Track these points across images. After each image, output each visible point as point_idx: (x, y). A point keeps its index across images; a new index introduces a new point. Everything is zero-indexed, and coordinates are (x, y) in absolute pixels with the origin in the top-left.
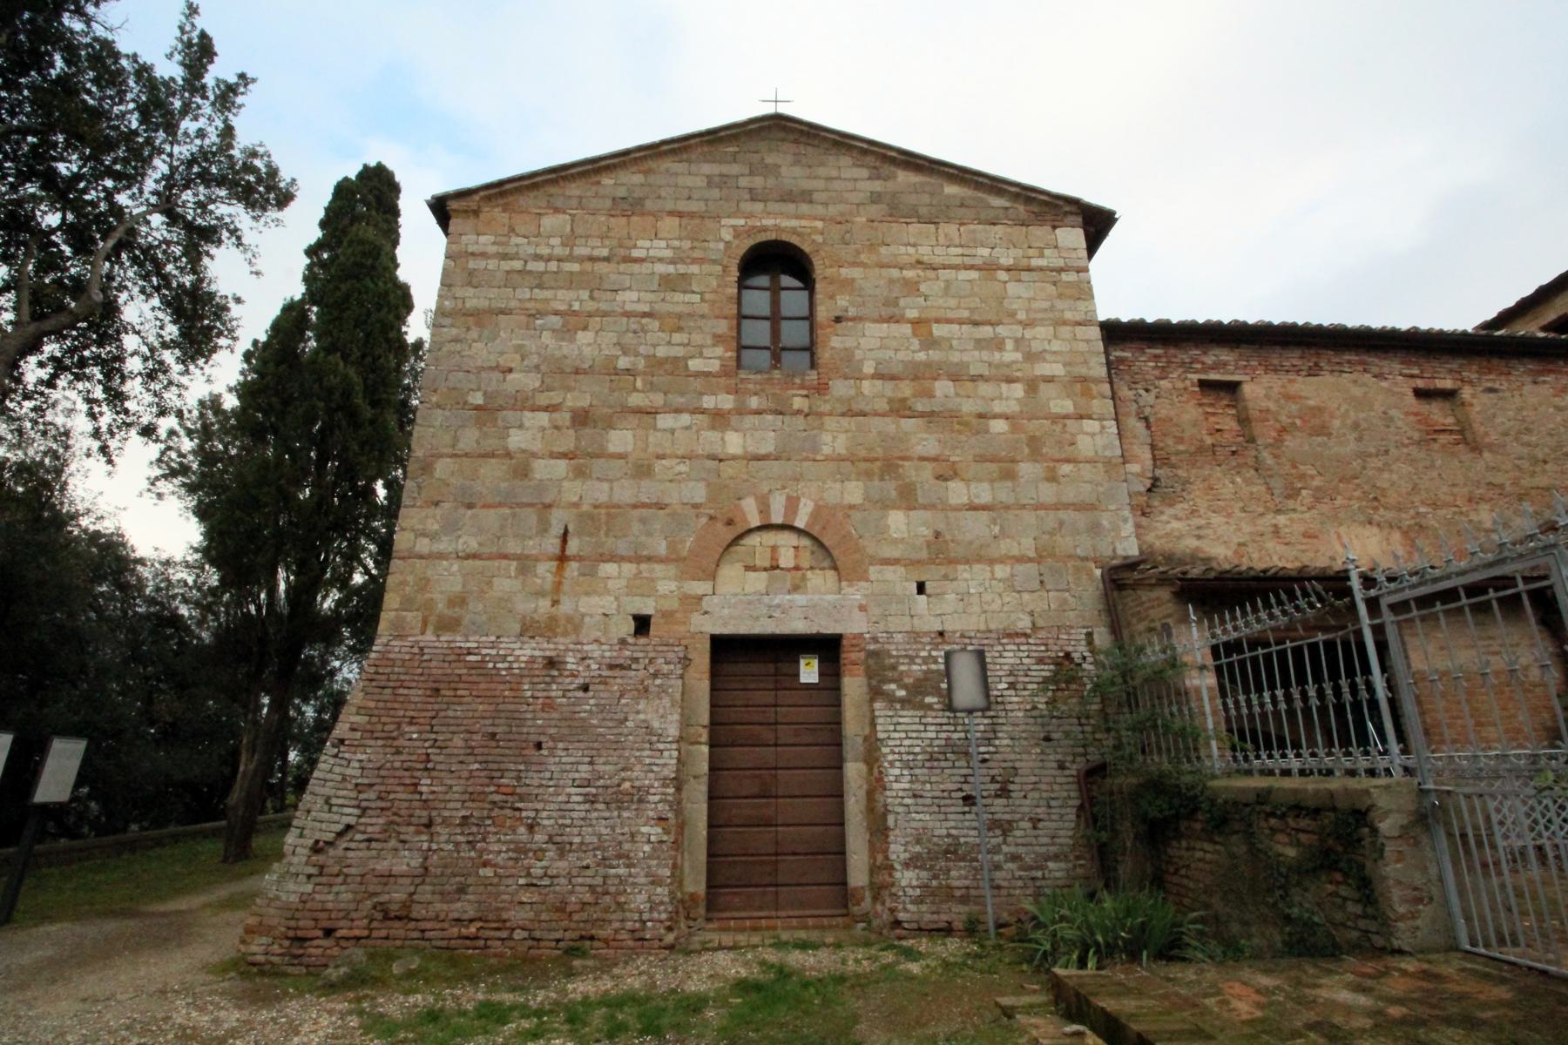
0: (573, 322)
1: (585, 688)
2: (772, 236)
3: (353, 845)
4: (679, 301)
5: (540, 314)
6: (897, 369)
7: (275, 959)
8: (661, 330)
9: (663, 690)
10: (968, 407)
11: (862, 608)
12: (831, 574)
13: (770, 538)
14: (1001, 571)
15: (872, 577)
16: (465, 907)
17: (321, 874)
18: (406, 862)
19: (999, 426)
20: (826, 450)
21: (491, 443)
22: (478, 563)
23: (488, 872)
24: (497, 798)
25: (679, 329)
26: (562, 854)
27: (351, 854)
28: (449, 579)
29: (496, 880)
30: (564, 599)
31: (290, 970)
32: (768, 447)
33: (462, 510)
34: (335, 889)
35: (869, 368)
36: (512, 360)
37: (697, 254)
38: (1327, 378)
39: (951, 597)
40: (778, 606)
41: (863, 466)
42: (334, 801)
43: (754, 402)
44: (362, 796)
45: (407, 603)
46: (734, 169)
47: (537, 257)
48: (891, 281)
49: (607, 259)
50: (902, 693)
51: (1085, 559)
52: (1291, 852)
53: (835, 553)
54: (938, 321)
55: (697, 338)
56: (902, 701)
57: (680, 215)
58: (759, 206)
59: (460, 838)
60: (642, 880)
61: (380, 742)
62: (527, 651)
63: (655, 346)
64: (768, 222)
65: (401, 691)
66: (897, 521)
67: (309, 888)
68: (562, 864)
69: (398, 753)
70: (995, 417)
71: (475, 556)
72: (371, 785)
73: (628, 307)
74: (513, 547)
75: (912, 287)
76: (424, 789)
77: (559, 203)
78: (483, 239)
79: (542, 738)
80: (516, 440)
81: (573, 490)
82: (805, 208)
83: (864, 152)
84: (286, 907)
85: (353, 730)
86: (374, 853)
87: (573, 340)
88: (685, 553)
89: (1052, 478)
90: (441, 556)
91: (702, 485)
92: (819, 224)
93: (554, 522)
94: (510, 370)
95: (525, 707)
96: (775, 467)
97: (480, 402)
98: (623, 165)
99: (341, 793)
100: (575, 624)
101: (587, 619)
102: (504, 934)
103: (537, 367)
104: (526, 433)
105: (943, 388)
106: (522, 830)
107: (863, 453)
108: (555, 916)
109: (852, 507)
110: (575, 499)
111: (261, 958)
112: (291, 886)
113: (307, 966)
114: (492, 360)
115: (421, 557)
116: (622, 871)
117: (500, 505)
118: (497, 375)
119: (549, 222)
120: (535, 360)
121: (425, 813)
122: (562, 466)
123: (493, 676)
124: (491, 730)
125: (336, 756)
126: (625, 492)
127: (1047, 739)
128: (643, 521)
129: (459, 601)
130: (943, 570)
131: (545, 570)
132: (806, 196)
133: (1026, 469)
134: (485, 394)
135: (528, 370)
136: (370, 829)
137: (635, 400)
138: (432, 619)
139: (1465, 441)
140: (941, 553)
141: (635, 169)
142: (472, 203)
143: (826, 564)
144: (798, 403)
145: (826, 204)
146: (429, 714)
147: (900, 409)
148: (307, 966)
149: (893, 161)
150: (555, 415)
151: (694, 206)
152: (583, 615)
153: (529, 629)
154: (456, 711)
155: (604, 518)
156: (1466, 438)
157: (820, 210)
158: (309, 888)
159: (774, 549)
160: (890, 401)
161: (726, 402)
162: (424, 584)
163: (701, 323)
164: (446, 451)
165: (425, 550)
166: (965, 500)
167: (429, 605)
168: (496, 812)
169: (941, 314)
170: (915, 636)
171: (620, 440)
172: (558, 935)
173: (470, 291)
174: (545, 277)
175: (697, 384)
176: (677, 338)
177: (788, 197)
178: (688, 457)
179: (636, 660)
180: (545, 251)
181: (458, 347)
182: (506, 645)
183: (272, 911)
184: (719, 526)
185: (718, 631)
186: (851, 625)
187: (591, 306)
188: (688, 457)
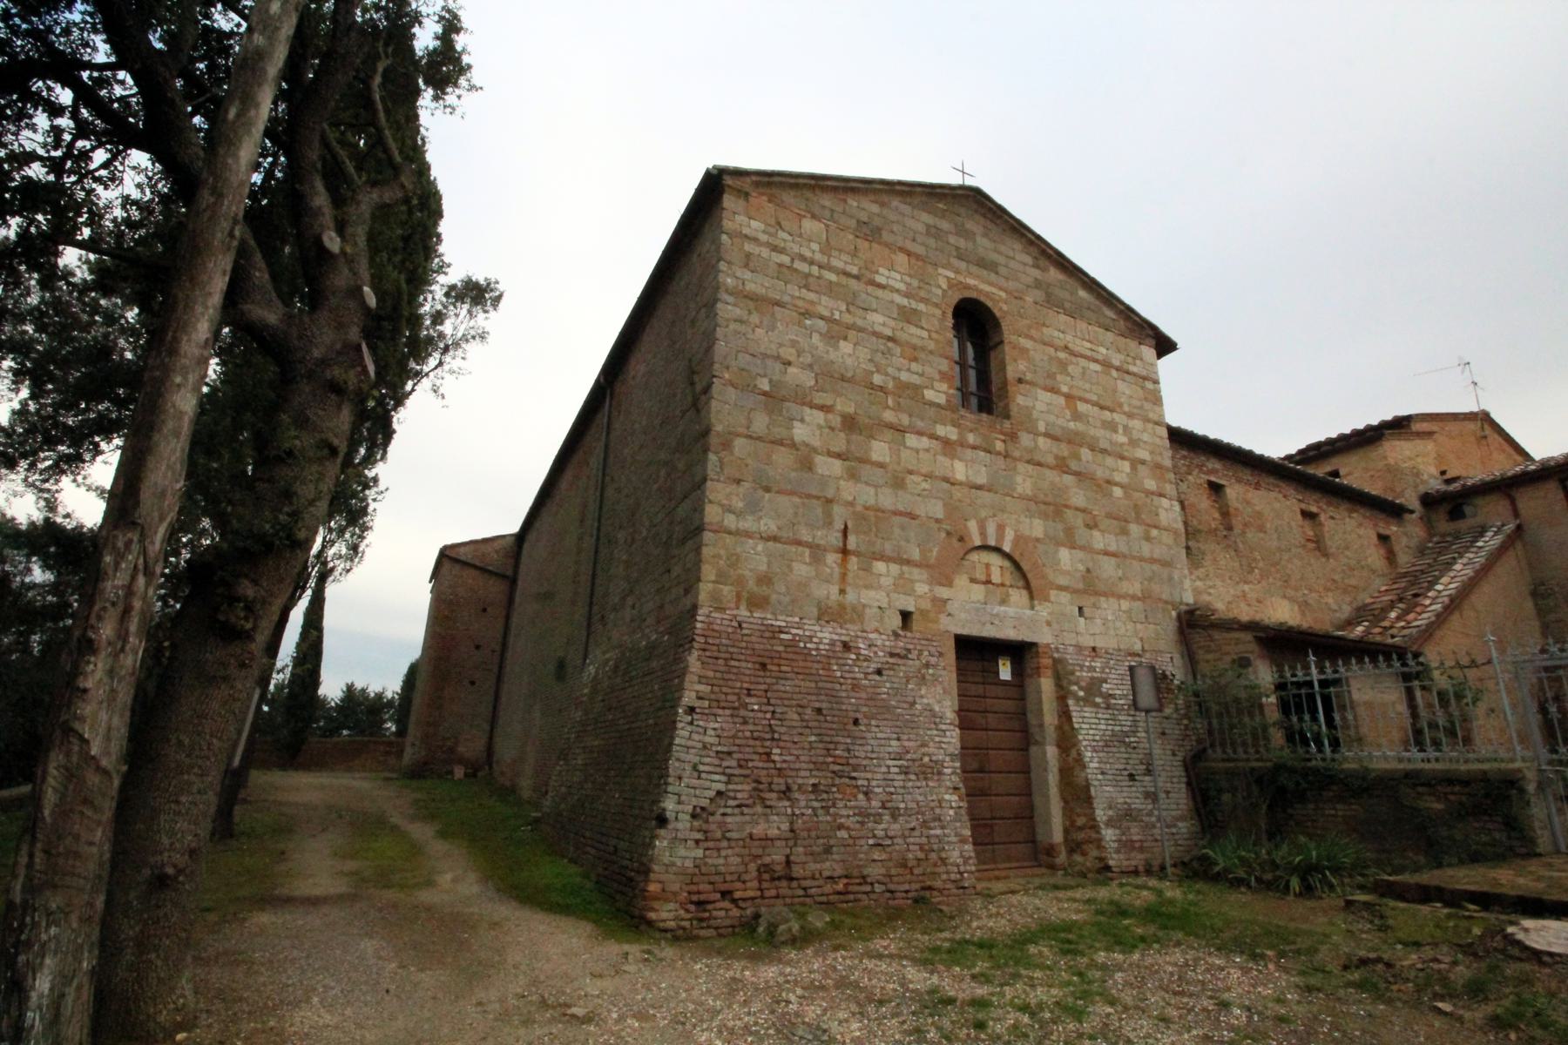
0: (836, 332)
1: (879, 672)
2: (974, 295)
3: (729, 811)
4: (914, 334)
5: (806, 314)
6: (1058, 432)
7: (686, 924)
8: (902, 356)
9: (935, 679)
10: (1100, 473)
11: (1049, 624)
12: (1024, 593)
13: (986, 557)
14: (1125, 605)
15: (1052, 599)
16: (830, 866)
17: (706, 840)
18: (776, 826)
19: (1118, 492)
20: (1020, 489)
21: (779, 432)
22: (779, 545)
23: (843, 834)
24: (837, 768)
25: (915, 359)
26: (894, 817)
27: (729, 819)
28: (757, 557)
29: (851, 842)
30: (848, 589)
31: (703, 933)
32: (982, 479)
33: (760, 492)
34: (723, 853)
35: (1042, 427)
36: (788, 353)
37: (922, 294)
38: (1262, 493)
39: (1098, 621)
40: (997, 615)
41: (1043, 507)
42: (701, 768)
43: (971, 438)
44: (725, 764)
45: (721, 578)
46: (945, 225)
47: (803, 258)
48: (1051, 358)
49: (857, 277)
50: (1081, 694)
51: (1166, 602)
52: (1439, 806)
53: (1029, 576)
54: (1081, 399)
55: (928, 370)
56: (1083, 699)
57: (909, 254)
58: (963, 265)
59: (816, 804)
60: (953, 839)
61: (728, 712)
62: (826, 635)
63: (899, 370)
64: (971, 282)
65: (733, 663)
66: (1064, 554)
67: (699, 853)
68: (896, 826)
69: (745, 723)
70: (1116, 484)
71: (775, 539)
72: (729, 753)
73: (878, 328)
74: (806, 536)
75: (1063, 365)
76: (776, 758)
77: (816, 210)
78: (754, 224)
79: (858, 715)
80: (800, 432)
81: (848, 490)
82: (993, 277)
83: (1031, 243)
84: (682, 872)
85: (700, 698)
86: (747, 818)
87: (836, 348)
88: (932, 561)
89: (1148, 538)
90: (748, 534)
91: (940, 504)
92: (1003, 294)
93: (837, 518)
94: (789, 363)
95: (838, 687)
96: (986, 497)
97: (767, 388)
98: (865, 192)
99: (707, 760)
100: (858, 613)
101: (867, 611)
102: (868, 888)
103: (811, 366)
104: (807, 428)
105: (1085, 453)
106: (861, 796)
107: (1042, 497)
108: (901, 871)
109: (1037, 540)
110: (850, 498)
111: (672, 924)
112: (682, 852)
113: (716, 928)
114: (773, 349)
115: (730, 533)
116: (938, 832)
117: (792, 493)
118: (778, 366)
119: (809, 225)
120: (809, 360)
121: (781, 781)
122: (837, 466)
123: (806, 654)
124: (817, 705)
125: (691, 723)
126: (887, 499)
127: (1163, 734)
128: (903, 528)
129: (765, 580)
130: (1093, 599)
131: (832, 558)
132: (992, 267)
133: (1135, 529)
134: (771, 381)
135: (803, 367)
136: (739, 795)
137: (888, 416)
138: (745, 594)
139: (1318, 549)
140: (1089, 589)
141: (872, 197)
142: (745, 184)
143: (1021, 583)
144: (999, 446)
145: (1007, 279)
146: (763, 687)
147: (1062, 466)
148: (716, 928)
149: (1049, 257)
150: (830, 416)
151: (920, 250)
152: (864, 606)
153: (827, 615)
154: (787, 686)
155: (872, 518)
156: (1318, 545)
157: (1002, 282)
158: (699, 853)
159: (988, 566)
160: (1056, 457)
161: (951, 433)
162: (735, 560)
163: (931, 358)
164: (740, 430)
165: (733, 527)
166: (1101, 546)
167: (740, 581)
168: (837, 781)
169: (1081, 394)
170: (1079, 648)
171: (879, 450)
172: (906, 887)
173: (748, 275)
174: (811, 280)
175: (932, 412)
176: (914, 366)
177: (983, 264)
178: (928, 476)
179: (909, 651)
180: (808, 254)
181: (742, 328)
182: (811, 627)
183: (673, 877)
184: (954, 541)
185: (960, 631)
186: (1044, 637)
187: (848, 319)
188: (928, 476)
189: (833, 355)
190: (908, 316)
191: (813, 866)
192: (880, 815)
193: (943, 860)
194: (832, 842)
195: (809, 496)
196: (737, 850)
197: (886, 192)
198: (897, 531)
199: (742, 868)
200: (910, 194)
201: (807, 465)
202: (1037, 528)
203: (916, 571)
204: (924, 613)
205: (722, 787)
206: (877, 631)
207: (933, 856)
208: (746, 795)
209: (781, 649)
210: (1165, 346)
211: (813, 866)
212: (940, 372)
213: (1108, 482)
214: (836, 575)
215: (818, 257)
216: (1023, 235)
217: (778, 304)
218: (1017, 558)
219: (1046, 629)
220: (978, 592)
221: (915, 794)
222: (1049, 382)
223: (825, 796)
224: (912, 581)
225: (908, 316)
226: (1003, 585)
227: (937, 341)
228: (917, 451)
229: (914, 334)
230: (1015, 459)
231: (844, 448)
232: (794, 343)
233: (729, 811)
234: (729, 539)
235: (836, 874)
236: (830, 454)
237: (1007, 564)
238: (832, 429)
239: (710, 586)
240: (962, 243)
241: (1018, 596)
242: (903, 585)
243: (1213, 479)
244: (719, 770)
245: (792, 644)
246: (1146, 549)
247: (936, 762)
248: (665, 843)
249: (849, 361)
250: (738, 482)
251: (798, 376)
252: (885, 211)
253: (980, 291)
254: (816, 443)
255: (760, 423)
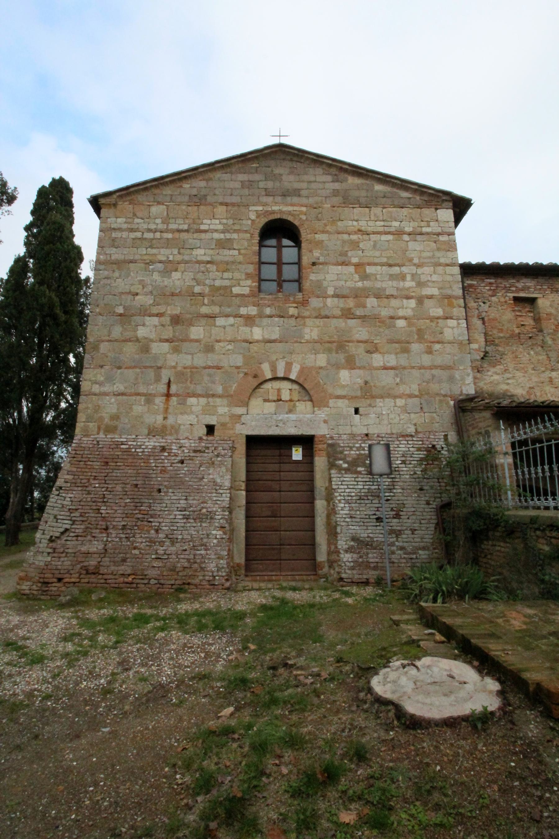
0: (170, 267)
1: (182, 462)
3: (69, 538)
4: (228, 254)
5: (152, 262)
6: (345, 292)
7: (35, 592)
9: (221, 463)
11: (325, 422)
14: (400, 402)
17: (54, 552)
18: (96, 546)
19: (401, 323)
20: (307, 337)
23: (136, 552)
25: (227, 270)
27: (68, 543)
28: (110, 406)
29: (141, 556)
32: (275, 336)
33: (115, 370)
34: (62, 559)
35: (330, 291)
36: (137, 288)
37: (237, 227)
41: (327, 345)
42: (59, 517)
43: (268, 311)
44: (72, 515)
45: (89, 419)
47: (149, 230)
48: (344, 242)
49: (187, 231)
51: (445, 396)
53: (312, 393)
54: (369, 264)
57: (227, 205)
58: (270, 199)
61: (80, 488)
62: (151, 443)
64: (276, 208)
65: (89, 463)
66: (344, 375)
67: (49, 559)
68: (173, 548)
70: (399, 318)
71: (123, 394)
72: (77, 510)
73: (199, 258)
74: (142, 389)
75: (355, 245)
76: (103, 511)
78: (119, 220)
79: (161, 487)
80: (142, 332)
81: (172, 359)
82: (295, 200)
83: (330, 166)
84: (38, 568)
86: (80, 542)
89: (429, 352)
90: (106, 394)
92: (304, 209)
93: (163, 376)
94: (137, 294)
95: (151, 472)
99: (62, 513)
100: (176, 429)
101: (182, 427)
103: (151, 292)
105: (371, 302)
106: (153, 532)
108: (170, 573)
109: (321, 368)
110: (173, 364)
111: (27, 592)
112: (40, 558)
113: (51, 596)
114: (127, 288)
115: (95, 395)
116: (203, 552)
118: (130, 297)
120: (150, 288)
121: (104, 523)
123: (135, 456)
124: (135, 482)
125: (58, 495)
126: (200, 360)
127: (421, 489)
128: (210, 375)
129: (115, 417)
130: (368, 402)
131: (159, 401)
132: (297, 193)
136: (77, 531)
137: (204, 310)
138: (103, 427)
141: (201, 178)
144: (292, 311)
147: (347, 314)
148: (51, 596)
149: (346, 171)
150: (162, 319)
152: (180, 425)
153: (152, 432)
155: (189, 374)
158: (49, 559)
159: (279, 390)
160: (342, 310)
161: (253, 311)
162: (97, 408)
163: (240, 266)
165: (97, 391)
167: (101, 419)
170: (353, 436)
171: (197, 332)
172: (173, 582)
175: (237, 301)
176: (226, 275)
180: (153, 227)
181: (108, 282)
183: (32, 570)
184: (250, 378)
186: (320, 430)
187: (179, 258)
189: (167, 282)
190: (222, 244)
191: (113, 568)
192: (164, 542)
193: (202, 569)
194: (128, 556)
195: (146, 367)
196: (70, 558)
197: (210, 171)
198: (206, 378)
199: (70, 568)
200: (228, 166)
201: (146, 349)
202: (322, 360)
203: (218, 401)
204: (223, 425)
205: (68, 527)
206: (187, 438)
207: (196, 565)
208: (81, 531)
209: (119, 453)
210: (460, 206)
211: (113, 568)
212: (247, 274)
213: (392, 318)
214: (162, 410)
215: (161, 226)
216: (322, 163)
217: (131, 262)
218: (301, 382)
219: (323, 425)
220: (270, 407)
221: (193, 530)
222: (341, 259)
223: (129, 531)
224: (216, 406)
225: (222, 244)
226: (291, 400)
227: (244, 255)
228: (224, 327)
229: (228, 254)
230: (304, 317)
231: (171, 336)
232: (141, 282)
233: (69, 538)
234: (94, 398)
235: (126, 573)
236: (161, 341)
237: (295, 387)
238: (163, 325)
239: (82, 424)
240: (270, 185)
241: (303, 407)
242: (209, 410)
243: (516, 295)
244: (69, 518)
245: (128, 450)
246: (426, 360)
247: (210, 512)
248: (32, 553)
249: (177, 283)
250: (102, 367)
251: (144, 300)
252: (210, 183)
253: (281, 212)
254: (153, 336)
255: (117, 332)
